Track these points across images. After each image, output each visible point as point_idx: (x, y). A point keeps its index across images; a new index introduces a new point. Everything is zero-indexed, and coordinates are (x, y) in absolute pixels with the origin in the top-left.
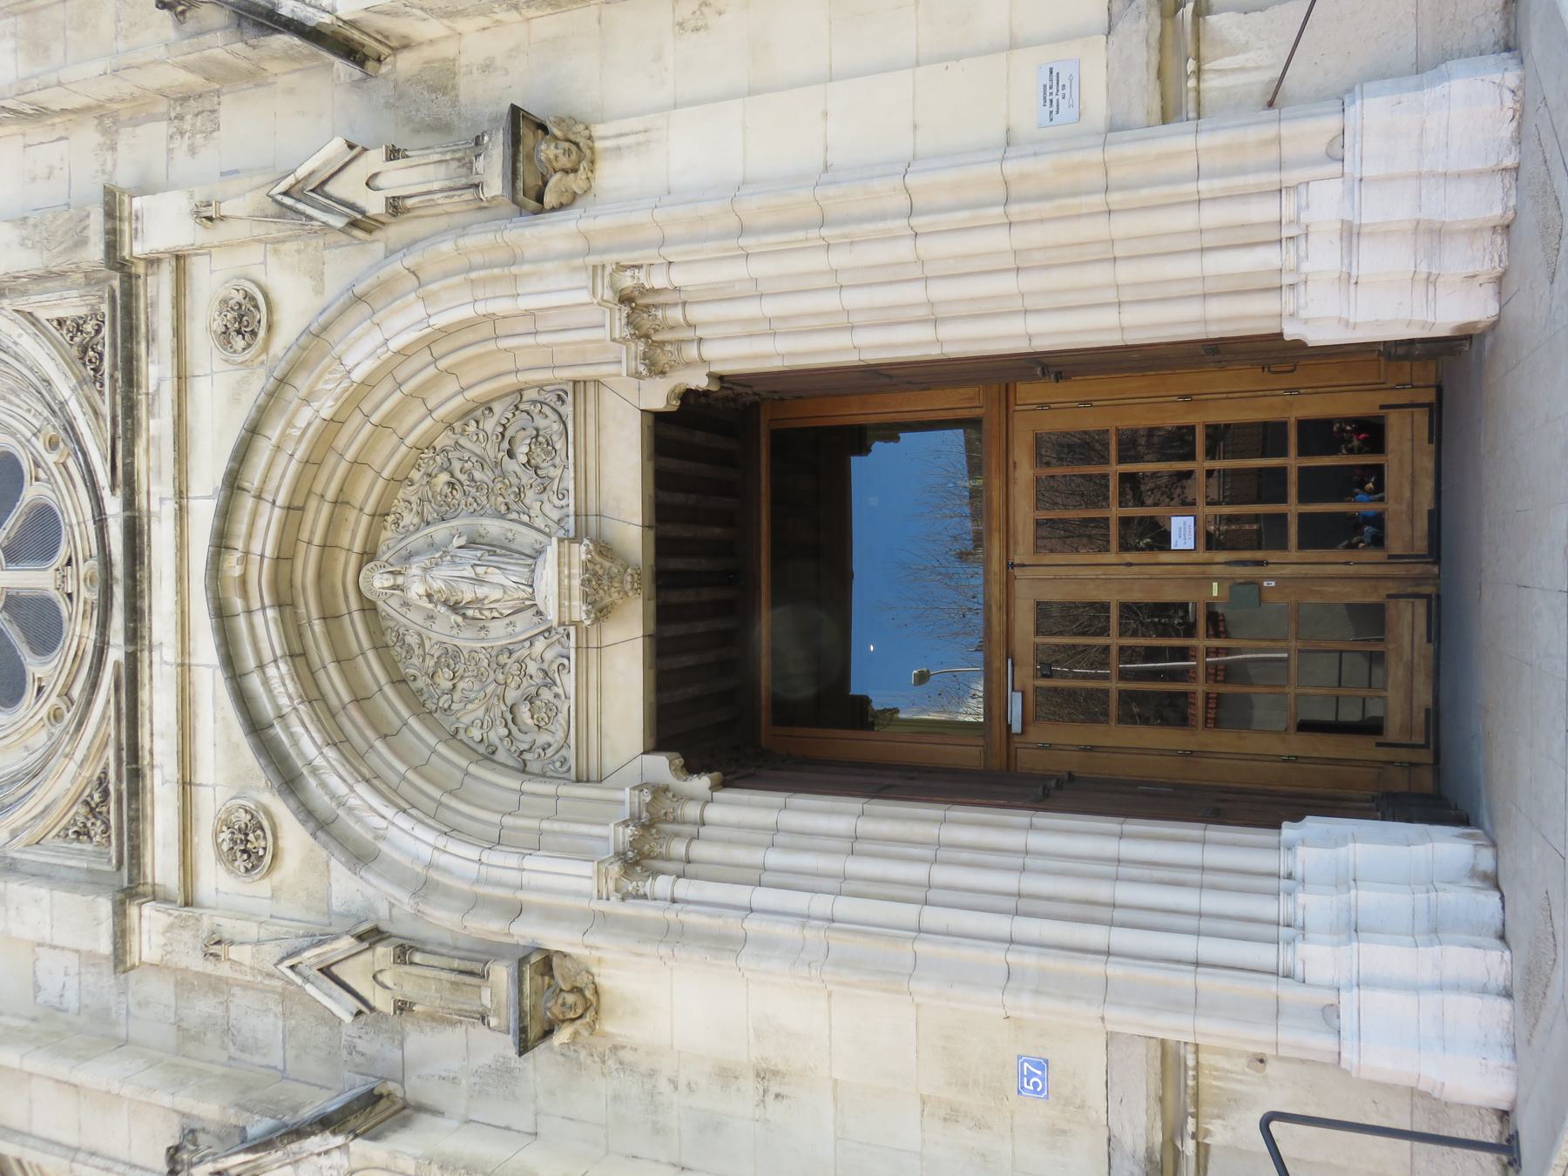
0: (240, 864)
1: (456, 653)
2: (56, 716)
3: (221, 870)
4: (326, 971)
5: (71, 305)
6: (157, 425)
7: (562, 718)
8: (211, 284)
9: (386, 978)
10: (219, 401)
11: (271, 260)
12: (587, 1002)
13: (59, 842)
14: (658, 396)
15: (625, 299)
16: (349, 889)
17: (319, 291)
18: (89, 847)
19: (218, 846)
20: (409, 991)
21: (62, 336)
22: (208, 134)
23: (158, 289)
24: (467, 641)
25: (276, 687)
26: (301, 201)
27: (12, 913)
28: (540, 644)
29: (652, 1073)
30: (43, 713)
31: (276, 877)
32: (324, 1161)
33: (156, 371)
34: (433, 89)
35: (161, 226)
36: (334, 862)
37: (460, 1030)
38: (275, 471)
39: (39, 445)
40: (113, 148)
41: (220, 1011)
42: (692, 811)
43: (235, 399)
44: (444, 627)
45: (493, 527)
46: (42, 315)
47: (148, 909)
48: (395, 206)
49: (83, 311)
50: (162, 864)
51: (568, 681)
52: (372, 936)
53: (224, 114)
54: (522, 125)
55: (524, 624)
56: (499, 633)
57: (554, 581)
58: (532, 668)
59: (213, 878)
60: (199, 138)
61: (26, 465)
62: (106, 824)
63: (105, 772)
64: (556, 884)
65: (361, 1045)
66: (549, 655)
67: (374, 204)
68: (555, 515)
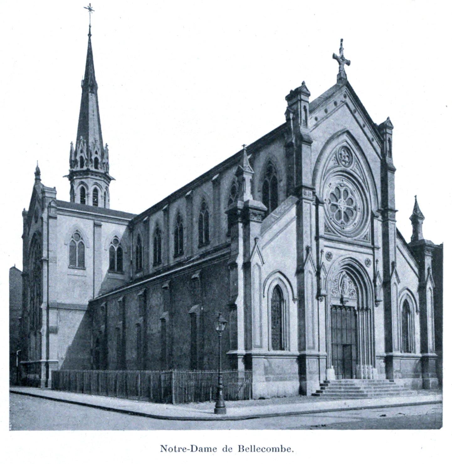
10: (362, 258)
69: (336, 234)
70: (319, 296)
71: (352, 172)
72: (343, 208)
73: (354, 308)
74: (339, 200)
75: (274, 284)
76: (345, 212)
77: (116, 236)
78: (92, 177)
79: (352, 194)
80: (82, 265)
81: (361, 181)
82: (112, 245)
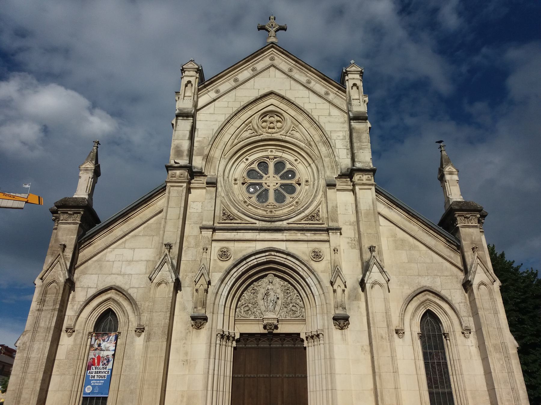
0: (220, 253)
1: (257, 293)
2: (245, 202)
3: (219, 248)
4: (203, 274)
5: (323, 214)
6: (299, 236)
7: (246, 316)
8: (324, 248)
9: (202, 287)
10: (302, 250)
11: (327, 261)
12: (198, 327)
13: (222, 208)
14: (303, 336)
15: (318, 336)
16: (216, 278)
17: (322, 272)
18: (221, 215)
19: (223, 248)
20: (200, 291)
21: (315, 212)
22: (351, 246)
23: (324, 237)
24: (260, 296)
25: (252, 261)
26: (336, 271)
27: (209, 201)
28: (259, 311)
29: (186, 339)
30: (246, 200)
31: (218, 260)
32: (170, 277)
33: (309, 236)
34: (356, 296)
35: (333, 237)
36: (221, 274)
37: (191, 299)
38: (290, 262)
39: (297, 200)
40: (350, 225)
41: (192, 246)
42: (230, 344)
43: (304, 253)
44: (262, 291)
45: (279, 302)
46: (320, 206)
47: (211, 233)
48: (335, 291)
49: (321, 216)
50: (219, 235)
51: (252, 318)
52: (209, 283)
53: (354, 250)
54: (346, 319)
55: (263, 308)
56: (261, 302)
57: (270, 315)
58: (255, 309)
59: (216, 246)
60: (350, 244)
61: (293, 195)
62: (225, 220)
63: (236, 220)
64: (218, 321)
65: (187, 278)
66: (257, 313)
67: (335, 287)
68: (282, 315)
69: (241, 219)
70: (199, 321)
71: (288, 139)
72: (271, 185)
73: (299, 334)
74: (278, 177)
75: (422, 311)
76: (275, 190)
79: (252, 163)
81: (302, 145)
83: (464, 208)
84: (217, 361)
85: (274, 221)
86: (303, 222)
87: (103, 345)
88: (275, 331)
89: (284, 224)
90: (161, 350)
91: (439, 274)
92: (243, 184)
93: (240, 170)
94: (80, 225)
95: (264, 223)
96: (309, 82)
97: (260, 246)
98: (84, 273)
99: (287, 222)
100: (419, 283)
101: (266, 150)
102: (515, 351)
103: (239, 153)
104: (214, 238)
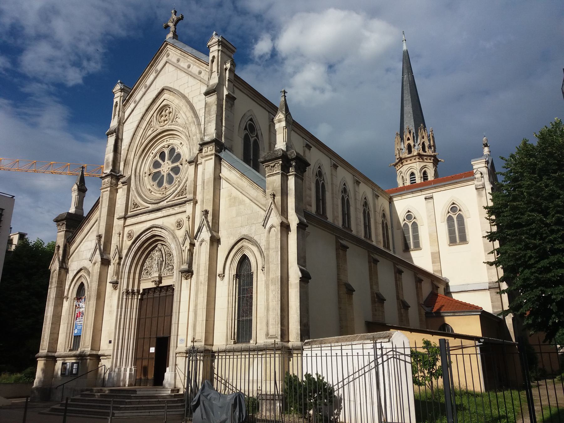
43: (172, 225)
77: (409, 212)
78: (407, 163)
80: (463, 239)
82: (449, 214)
83: (267, 159)
84: (123, 310)
85: (159, 203)
86: (176, 198)
87: (80, 304)
88: (161, 285)
89: (164, 203)
90: (278, 282)
91: (255, 222)
92: (149, 175)
93: (147, 166)
94: (282, 174)
95: (154, 205)
96: (189, 67)
97: (148, 225)
98: (72, 261)
99: (166, 201)
100: (240, 233)
101: (163, 141)
102: (298, 281)
103: (145, 151)
104: (126, 224)
